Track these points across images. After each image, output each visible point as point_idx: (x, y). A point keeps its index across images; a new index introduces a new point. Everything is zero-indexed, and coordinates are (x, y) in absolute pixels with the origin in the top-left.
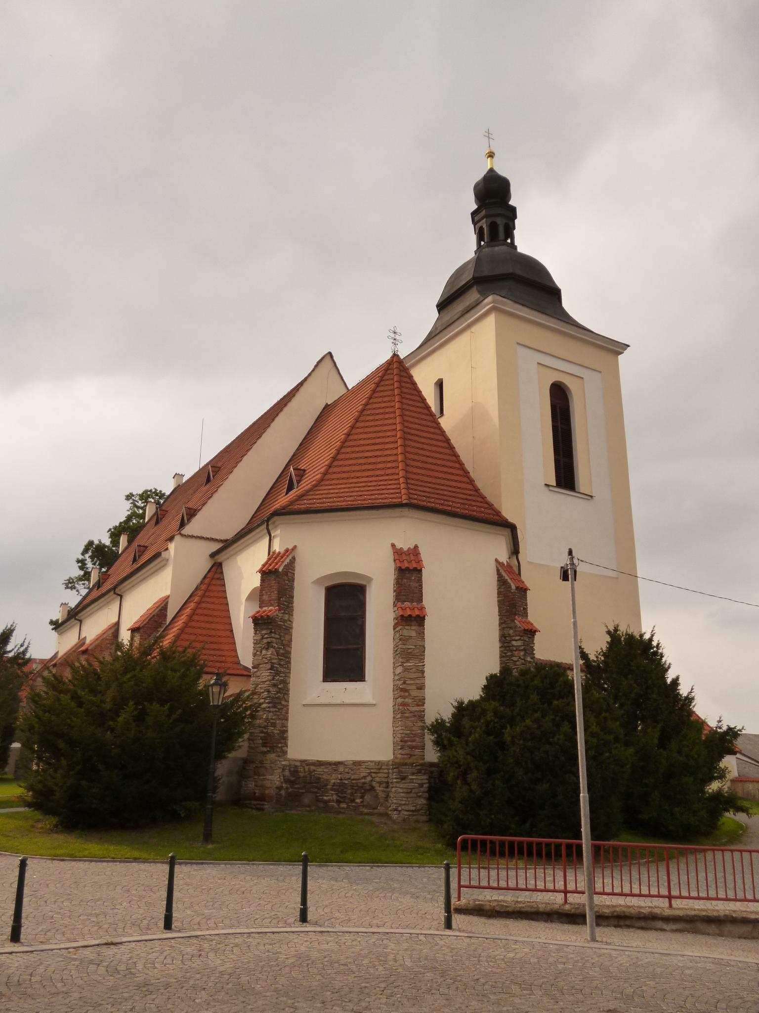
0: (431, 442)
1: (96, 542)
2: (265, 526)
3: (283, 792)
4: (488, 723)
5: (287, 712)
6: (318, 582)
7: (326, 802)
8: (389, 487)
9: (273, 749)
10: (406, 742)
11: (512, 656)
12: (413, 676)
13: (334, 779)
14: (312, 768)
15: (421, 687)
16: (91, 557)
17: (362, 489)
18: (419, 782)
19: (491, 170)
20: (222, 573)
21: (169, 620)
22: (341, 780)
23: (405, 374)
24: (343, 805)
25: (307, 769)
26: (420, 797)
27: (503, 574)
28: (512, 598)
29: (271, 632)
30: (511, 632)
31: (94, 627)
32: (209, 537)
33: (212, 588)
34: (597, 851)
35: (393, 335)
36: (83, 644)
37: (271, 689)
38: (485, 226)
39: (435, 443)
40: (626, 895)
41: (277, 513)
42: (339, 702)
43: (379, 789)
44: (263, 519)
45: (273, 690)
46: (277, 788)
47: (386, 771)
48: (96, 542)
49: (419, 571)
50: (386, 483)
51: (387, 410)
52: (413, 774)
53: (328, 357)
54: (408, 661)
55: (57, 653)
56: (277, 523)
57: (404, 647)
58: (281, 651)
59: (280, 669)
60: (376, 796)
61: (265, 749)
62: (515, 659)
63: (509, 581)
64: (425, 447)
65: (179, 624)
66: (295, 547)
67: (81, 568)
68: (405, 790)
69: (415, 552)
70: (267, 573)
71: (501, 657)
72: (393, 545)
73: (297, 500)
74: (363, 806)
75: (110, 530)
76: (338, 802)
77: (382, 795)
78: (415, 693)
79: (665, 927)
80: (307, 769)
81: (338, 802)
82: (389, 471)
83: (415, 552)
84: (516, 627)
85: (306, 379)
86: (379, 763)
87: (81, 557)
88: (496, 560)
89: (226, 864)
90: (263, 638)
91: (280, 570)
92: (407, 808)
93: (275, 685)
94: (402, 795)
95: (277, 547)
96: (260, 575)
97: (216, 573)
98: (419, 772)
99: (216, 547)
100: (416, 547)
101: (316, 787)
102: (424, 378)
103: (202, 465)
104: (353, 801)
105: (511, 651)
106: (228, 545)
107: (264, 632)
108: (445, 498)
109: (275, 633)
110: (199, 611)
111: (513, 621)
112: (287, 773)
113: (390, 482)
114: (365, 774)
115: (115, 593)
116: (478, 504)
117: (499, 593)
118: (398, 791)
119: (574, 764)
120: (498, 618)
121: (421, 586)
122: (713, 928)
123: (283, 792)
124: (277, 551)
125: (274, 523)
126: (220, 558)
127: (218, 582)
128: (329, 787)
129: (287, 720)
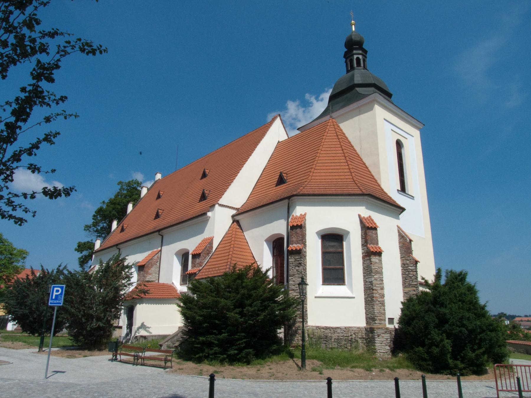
6: (318, 233)
12: (379, 283)
13: (335, 336)
15: (382, 289)
30: (408, 262)
32: (230, 206)
52: (383, 333)
71: (402, 274)
72: (359, 216)
86: (359, 328)
99: (234, 212)
107: (297, 257)
117: (400, 243)
120: (400, 255)
121: (377, 236)
128: (333, 340)
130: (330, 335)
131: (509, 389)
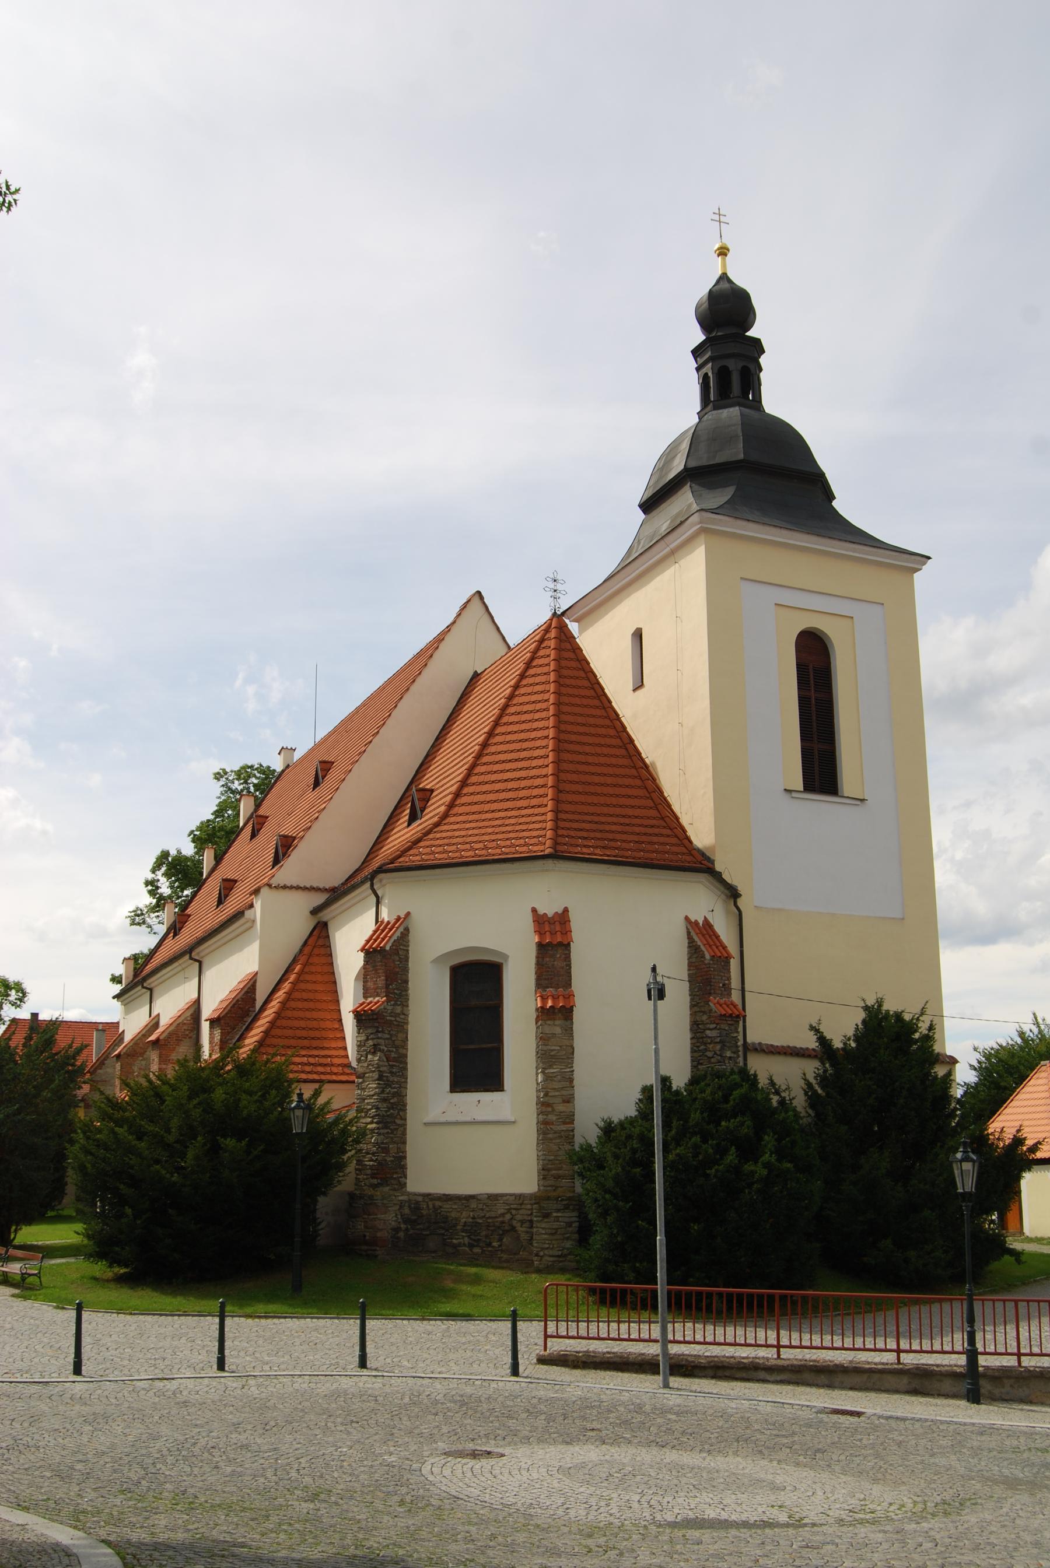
0: (598, 750)
1: (173, 852)
2: (368, 884)
3: (401, 1234)
4: (634, 1151)
5: (404, 1133)
6: (439, 960)
7: (455, 1246)
8: (531, 826)
9: (385, 1182)
10: (549, 1170)
11: (706, 1050)
12: (557, 1085)
13: (465, 1217)
14: (438, 1203)
15: (569, 1100)
16: (165, 874)
17: (497, 830)
18: (567, 1220)
19: (724, 277)
20: (328, 937)
21: (259, 1004)
22: (474, 1218)
23: (568, 646)
24: (477, 1250)
25: (431, 1206)
26: (568, 1239)
27: (696, 938)
28: (711, 968)
29: (378, 1031)
30: (705, 1018)
31: (170, 1004)
33: (314, 960)
34: (678, 1294)
35: (552, 585)
36: (156, 1025)
37: (380, 1105)
38: (710, 374)
39: (605, 750)
40: (689, 1343)
41: (381, 870)
42: (468, 1119)
43: (521, 1229)
44: (370, 873)
45: (383, 1106)
46: (393, 1229)
47: (529, 1207)
48: (173, 852)
49: (567, 946)
50: (528, 819)
51: (538, 706)
52: (558, 1211)
53: (476, 600)
54: (550, 1067)
55: (13, 1296)
56: (384, 881)
57: (545, 1048)
58: (393, 1055)
59: (391, 1079)
60: (518, 1238)
61: (375, 1181)
62: (710, 1054)
63: (702, 947)
64: (590, 759)
65: (274, 1005)
66: (408, 914)
67: (152, 893)
68: (550, 1231)
69: (563, 919)
70: (372, 953)
71: (693, 1051)
73: (410, 848)
74: (502, 1251)
75: (192, 832)
76: (471, 1246)
77: (524, 1237)
78: (561, 1108)
79: (768, 1378)
80: (431, 1206)
81: (471, 1246)
82: (534, 802)
83: (563, 919)
84: (711, 1011)
85: (449, 628)
87: (150, 876)
88: (687, 918)
89: (312, 1318)
90: (367, 1039)
91: (388, 948)
92: (551, 1252)
93: (385, 1100)
94: (546, 1236)
95: (385, 915)
96: (362, 954)
97: (319, 937)
98: (566, 1207)
99: (319, 899)
100: (566, 910)
101: (443, 1228)
102: (603, 647)
103: (321, 734)
104: (489, 1245)
105: (705, 1044)
106: (336, 894)
107: (370, 1031)
108: (610, 836)
109: (383, 1032)
110: (296, 995)
111: (707, 1003)
112: (407, 1211)
113: (534, 819)
114: (502, 1211)
115: (191, 958)
116: (662, 839)
117: (690, 965)
118: (542, 1228)
119: (809, 1190)
120: (688, 998)
121: (569, 966)
122: (823, 1379)
123: (401, 1234)
124: (386, 920)
125: (381, 881)
126: (325, 915)
127: (322, 951)
128: (459, 1227)
129: (405, 1143)
130: (453, 1215)
131: (992, 1349)
